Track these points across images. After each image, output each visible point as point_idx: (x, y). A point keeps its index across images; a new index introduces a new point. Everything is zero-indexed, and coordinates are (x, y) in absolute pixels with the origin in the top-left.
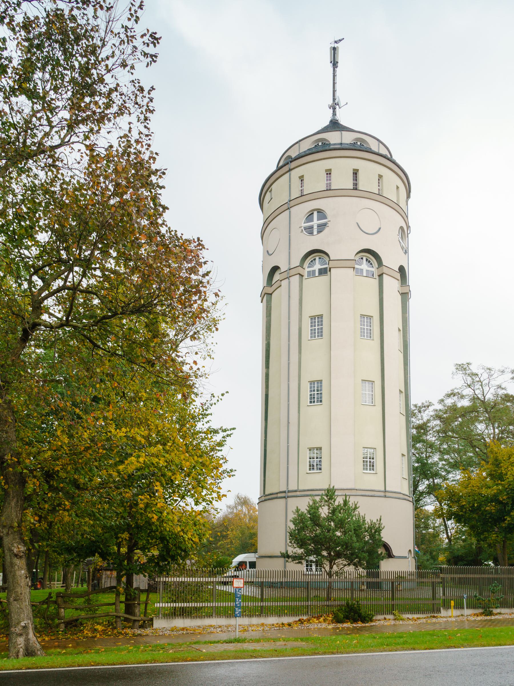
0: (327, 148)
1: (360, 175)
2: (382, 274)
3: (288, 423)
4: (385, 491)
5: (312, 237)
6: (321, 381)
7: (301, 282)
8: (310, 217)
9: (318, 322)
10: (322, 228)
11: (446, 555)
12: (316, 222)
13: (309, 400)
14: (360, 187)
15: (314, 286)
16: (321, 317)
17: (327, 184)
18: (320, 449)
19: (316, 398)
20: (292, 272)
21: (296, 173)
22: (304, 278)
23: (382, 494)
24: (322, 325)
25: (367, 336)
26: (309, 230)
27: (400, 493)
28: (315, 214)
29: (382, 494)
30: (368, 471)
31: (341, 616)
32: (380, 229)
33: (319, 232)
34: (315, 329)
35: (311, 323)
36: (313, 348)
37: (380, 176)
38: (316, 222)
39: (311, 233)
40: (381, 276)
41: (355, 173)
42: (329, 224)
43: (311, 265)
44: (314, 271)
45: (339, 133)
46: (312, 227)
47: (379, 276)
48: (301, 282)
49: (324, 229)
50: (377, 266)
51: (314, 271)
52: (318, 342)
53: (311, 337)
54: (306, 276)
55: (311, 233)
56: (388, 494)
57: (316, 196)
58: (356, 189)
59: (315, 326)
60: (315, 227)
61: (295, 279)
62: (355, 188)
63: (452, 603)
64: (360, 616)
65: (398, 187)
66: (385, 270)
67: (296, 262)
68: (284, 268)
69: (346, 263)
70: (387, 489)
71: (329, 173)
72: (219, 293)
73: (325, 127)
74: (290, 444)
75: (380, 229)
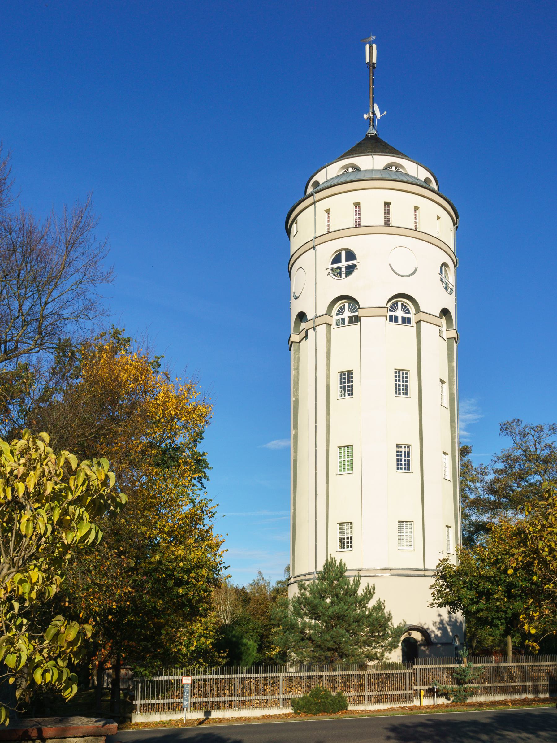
1: (392, 207)
2: (420, 321)
3: (316, 494)
8: (337, 259)
9: (348, 378)
10: (350, 270)
11: (435, 640)
12: (344, 263)
14: (393, 222)
15: (344, 335)
16: (350, 373)
20: (318, 321)
21: (321, 206)
24: (352, 382)
26: (337, 273)
28: (343, 254)
32: (416, 269)
33: (347, 276)
35: (341, 379)
38: (344, 263)
42: (358, 266)
43: (340, 312)
44: (343, 320)
47: (416, 323)
49: (352, 271)
50: (414, 312)
52: (348, 400)
57: (342, 234)
60: (344, 269)
61: (322, 330)
67: (322, 309)
68: (310, 316)
70: (426, 568)
73: (298, 405)
75: (416, 269)
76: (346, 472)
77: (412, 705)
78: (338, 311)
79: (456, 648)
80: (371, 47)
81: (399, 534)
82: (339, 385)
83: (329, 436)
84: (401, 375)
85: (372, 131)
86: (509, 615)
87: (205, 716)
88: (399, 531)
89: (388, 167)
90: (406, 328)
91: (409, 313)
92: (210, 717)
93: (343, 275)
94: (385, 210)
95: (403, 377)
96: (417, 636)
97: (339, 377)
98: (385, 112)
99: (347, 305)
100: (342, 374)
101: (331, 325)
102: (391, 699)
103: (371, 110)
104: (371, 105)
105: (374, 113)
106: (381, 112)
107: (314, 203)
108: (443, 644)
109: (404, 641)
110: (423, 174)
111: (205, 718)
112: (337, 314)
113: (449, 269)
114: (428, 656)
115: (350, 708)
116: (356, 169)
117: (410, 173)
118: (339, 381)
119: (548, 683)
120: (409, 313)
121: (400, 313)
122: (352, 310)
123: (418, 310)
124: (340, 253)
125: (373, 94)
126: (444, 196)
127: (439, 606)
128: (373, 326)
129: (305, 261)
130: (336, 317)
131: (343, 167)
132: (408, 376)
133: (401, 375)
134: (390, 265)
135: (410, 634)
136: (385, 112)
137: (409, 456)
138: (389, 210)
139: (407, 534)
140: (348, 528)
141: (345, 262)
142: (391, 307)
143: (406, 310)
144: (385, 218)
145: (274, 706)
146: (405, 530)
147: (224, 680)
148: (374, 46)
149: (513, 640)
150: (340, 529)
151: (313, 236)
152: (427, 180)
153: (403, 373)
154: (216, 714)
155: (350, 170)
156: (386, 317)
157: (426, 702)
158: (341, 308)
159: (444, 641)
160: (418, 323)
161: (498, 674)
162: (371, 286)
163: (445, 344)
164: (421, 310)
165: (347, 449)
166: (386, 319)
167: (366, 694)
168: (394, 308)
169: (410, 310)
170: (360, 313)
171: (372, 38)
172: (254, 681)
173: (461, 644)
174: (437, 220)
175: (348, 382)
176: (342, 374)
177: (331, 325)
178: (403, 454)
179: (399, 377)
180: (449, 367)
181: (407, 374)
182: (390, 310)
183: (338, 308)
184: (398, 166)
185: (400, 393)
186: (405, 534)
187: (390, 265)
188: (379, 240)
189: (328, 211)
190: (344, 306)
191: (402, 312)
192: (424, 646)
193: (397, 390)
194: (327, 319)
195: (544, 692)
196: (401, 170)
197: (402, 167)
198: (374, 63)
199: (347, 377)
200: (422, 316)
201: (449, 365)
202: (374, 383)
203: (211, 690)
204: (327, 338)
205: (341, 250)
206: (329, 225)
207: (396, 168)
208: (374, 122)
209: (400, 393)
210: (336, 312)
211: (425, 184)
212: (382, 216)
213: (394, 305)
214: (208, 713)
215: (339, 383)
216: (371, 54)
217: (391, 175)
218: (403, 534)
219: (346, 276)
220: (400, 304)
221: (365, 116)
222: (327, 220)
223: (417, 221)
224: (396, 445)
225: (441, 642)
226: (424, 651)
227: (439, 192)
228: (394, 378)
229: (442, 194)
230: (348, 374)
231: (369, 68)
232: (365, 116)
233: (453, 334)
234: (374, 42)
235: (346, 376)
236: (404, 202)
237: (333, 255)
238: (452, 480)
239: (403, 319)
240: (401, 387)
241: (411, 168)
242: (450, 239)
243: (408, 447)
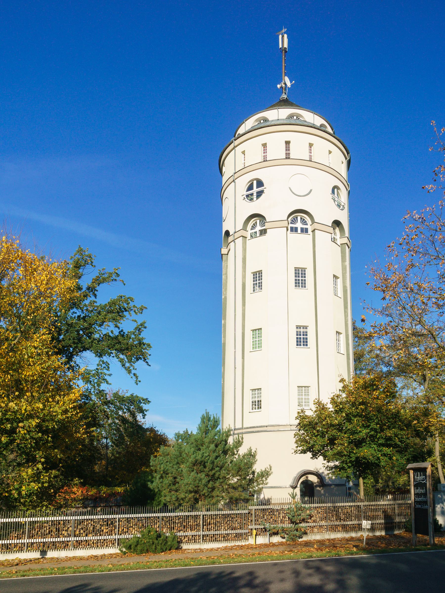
0: (268, 124)
5: (252, 204)
7: (244, 244)
8: (250, 188)
10: (259, 194)
11: (329, 482)
12: (255, 190)
17: (264, 156)
20: (237, 235)
21: (239, 149)
22: (247, 239)
25: (302, 287)
26: (249, 197)
28: (255, 183)
30: (257, 410)
32: (311, 191)
35: (254, 278)
37: (311, 145)
38: (255, 190)
39: (251, 200)
43: (253, 227)
44: (256, 232)
46: (252, 194)
48: (244, 244)
49: (260, 195)
55: (251, 200)
58: (289, 158)
61: (239, 241)
62: (288, 157)
67: (240, 226)
69: (277, 223)
71: (265, 145)
72: (429, 264)
75: (311, 191)
76: (257, 350)
77: (247, 543)
78: (252, 227)
79: (350, 488)
80: (283, 37)
81: (299, 397)
82: (253, 283)
83: (244, 322)
84: (300, 272)
85: (284, 96)
86: (353, 459)
87: (41, 555)
88: (299, 395)
89: (291, 116)
90: (304, 236)
91: (307, 224)
92: (46, 557)
93: (255, 199)
94: (286, 147)
95: (302, 274)
96: (313, 479)
97: (252, 277)
98: (294, 82)
99: (258, 221)
100: (255, 274)
101: (246, 238)
102: (226, 538)
103: (283, 82)
104: (283, 78)
105: (285, 84)
106: (291, 82)
107: (234, 148)
108: (336, 485)
109: (302, 483)
110: (318, 121)
111: (41, 557)
112: (252, 229)
113: (341, 191)
114: (323, 495)
115: (185, 546)
116: (266, 120)
117: (307, 121)
118: (252, 280)
119: (383, 521)
120: (307, 224)
121: (299, 225)
122: (263, 224)
123: (313, 221)
124: (252, 183)
125: (285, 70)
126: (346, 145)
127: (301, 453)
128: (277, 235)
129: (228, 193)
130: (250, 232)
131: (256, 120)
132: (306, 272)
133: (300, 272)
134: (290, 188)
135: (307, 478)
136: (294, 82)
137: (306, 335)
138: (289, 147)
139: (305, 397)
140: (258, 394)
141: (256, 189)
142: (292, 221)
143: (304, 222)
144: (286, 154)
145: (111, 545)
146: (304, 393)
147: (62, 522)
148: (286, 36)
149: (365, 481)
150: (252, 394)
151: (234, 172)
152: (322, 125)
153: (302, 271)
154: (51, 554)
155: (262, 121)
156: (287, 228)
157: (262, 540)
158: (254, 224)
159: (338, 482)
160: (313, 231)
161: (335, 512)
162: (276, 206)
163: (339, 249)
164: (316, 221)
165: (257, 331)
166: (287, 230)
167: (201, 533)
168: (294, 221)
169: (308, 222)
170: (267, 226)
171: (283, 31)
172: (92, 522)
173: (354, 485)
174: (337, 160)
175: (259, 280)
176: (255, 274)
177: (246, 238)
178: (302, 333)
179: (299, 273)
180: (342, 266)
181: (305, 271)
182: (291, 223)
183: (252, 224)
184: (298, 116)
185: (299, 286)
186: (304, 397)
187: (290, 188)
188: (287, 171)
189: (243, 153)
190: (256, 223)
191: (301, 224)
192: (320, 487)
193: (297, 284)
194: (243, 233)
195: (381, 529)
196: (301, 119)
197: (301, 116)
198: (286, 48)
199: (258, 276)
200: (316, 226)
201: (342, 264)
202: (278, 279)
203: (49, 531)
204: (243, 247)
205: (252, 180)
206: (244, 163)
207: (297, 118)
208: (285, 90)
209: (299, 286)
210: (250, 227)
211: (321, 128)
212: (284, 152)
213: (294, 219)
214: (43, 553)
215: (252, 281)
216: (284, 41)
217: (292, 121)
218: (302, 397)
219: (257, 199)
220: (299, 218)
221: (279, 86)
222: (243, 159)
223: (312, 154)
224: (296, 327)
225: (335, 483)
226: (319, 491)
227: (334, 135)
228: (294, 275)
229: (337, 137)
230: (259, 274)
231: (282, 52)
232: (279, 86)
233: (345, 240)
234: (285, 33)
235: (258, 276)
236: (300, 141)
237: (247, 184)
238: (345, 354)
239: (302, 230)
240: (300, 282)
241: (309, 116)
242: (343, 170)
243: (306, 328)
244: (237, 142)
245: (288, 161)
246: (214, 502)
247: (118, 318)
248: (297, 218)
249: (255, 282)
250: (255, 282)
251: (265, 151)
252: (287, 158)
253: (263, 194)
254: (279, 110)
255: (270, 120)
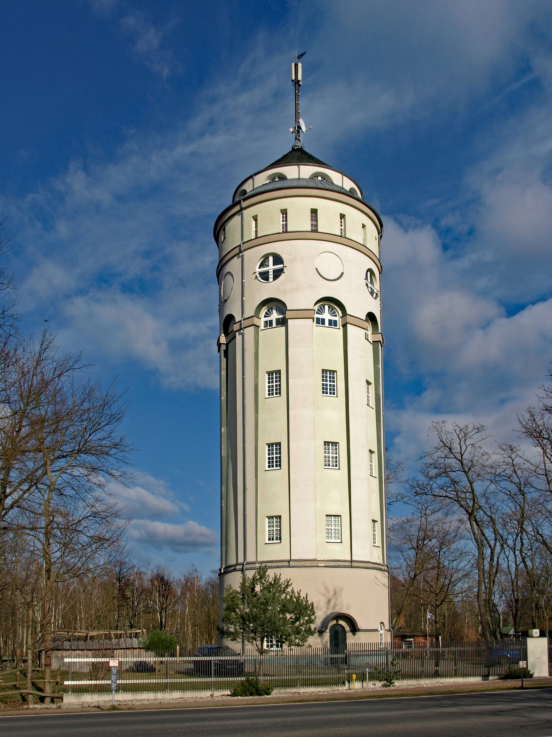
4: (352, 561)
5: (267, 285)
6: (280, 444)
9: (276, 378)
10: (277, 274)
13: (267, 464)
18: (280, 517)
19: (275, 462)
22: (260, 329)
23: (349, 564)
25: (330, 393)
26: (265, 276)
27: (369, 562)
28: (271, 259)
29: (349, 564)
31: (239, 689)
32: (342, 274)
34: (273, 386)
36: (271, 407)
37: (342, 216)
38: (271, 267)
39: (267, 279)
40: (344, 326)
41: (314, 212)
44: (271, 322)
45: (296, 167)
49: (280, 275)
51: (271, 322)
53: (269, 394)
54: (262, 327)
56: (354, 564)
59: (273, 382)
62: (315, 229)
63: (354, 676)
64: (257, 690)
65: (364, 226)
66: (349, 319)
67: (250, 311)
71: (284, 212)
74: (254, 479)
75: (342, 274)
78: (266, 313)
101: (259, 327)
110: (348, 184)
112: (265, 317)
116: (282, 177)
131: (269, 177)
152: (352, 190)
156: (313, 319)
166: (313, 321)
168: (321, 311)
177: (259, 327)
182: (317, 313)
184: (325, 177)
185: (327, 393)
189: (255, 218)
199: (328, 389)
204: (255, 339)
209: (327, 393)
210: (264, 314)
233: (379, 338)
238: (377, 476)
244: (244, 204)
245: (315, 235)
246: (18, 686)
247: (477, 469)
248: (324, 306)
249: (271, 384)
250: (271, 384)
251: (285, 219)
252: (312, 231)
253: (283, 275)
254: (300, 166)
255: (288, 178)
